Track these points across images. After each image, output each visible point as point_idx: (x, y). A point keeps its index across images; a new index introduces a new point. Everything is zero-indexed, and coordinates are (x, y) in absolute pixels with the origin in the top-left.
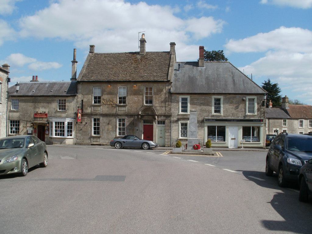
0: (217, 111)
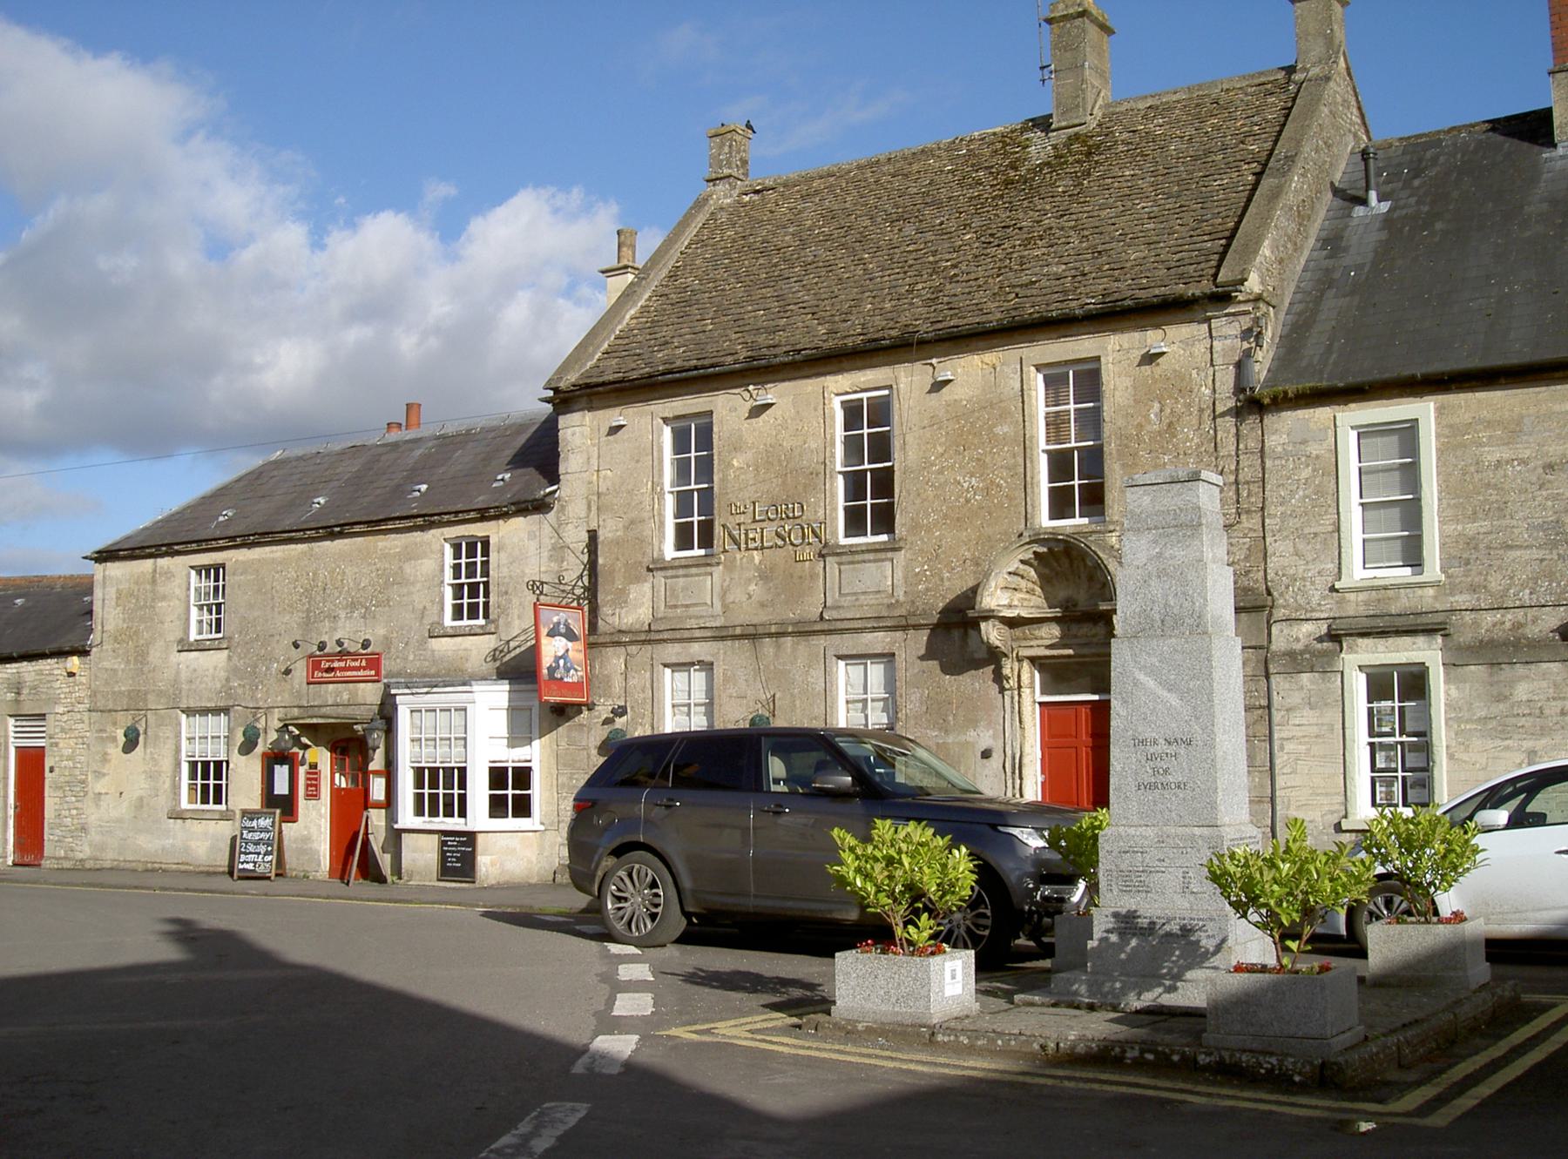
0: (871, 427)
